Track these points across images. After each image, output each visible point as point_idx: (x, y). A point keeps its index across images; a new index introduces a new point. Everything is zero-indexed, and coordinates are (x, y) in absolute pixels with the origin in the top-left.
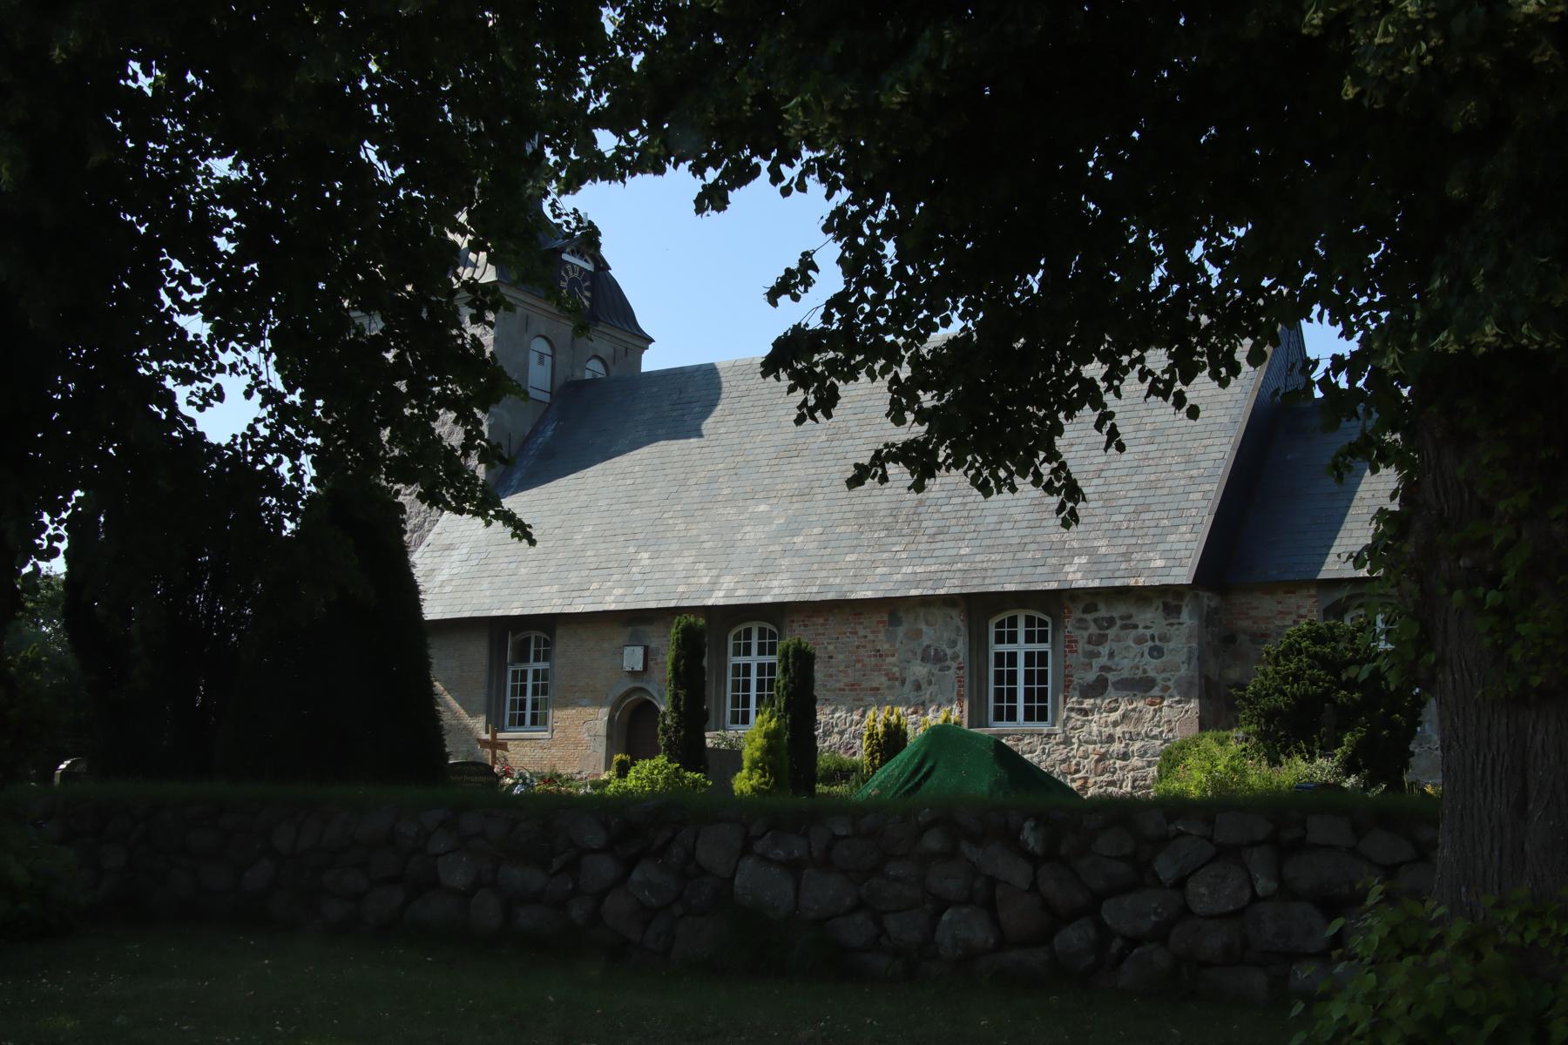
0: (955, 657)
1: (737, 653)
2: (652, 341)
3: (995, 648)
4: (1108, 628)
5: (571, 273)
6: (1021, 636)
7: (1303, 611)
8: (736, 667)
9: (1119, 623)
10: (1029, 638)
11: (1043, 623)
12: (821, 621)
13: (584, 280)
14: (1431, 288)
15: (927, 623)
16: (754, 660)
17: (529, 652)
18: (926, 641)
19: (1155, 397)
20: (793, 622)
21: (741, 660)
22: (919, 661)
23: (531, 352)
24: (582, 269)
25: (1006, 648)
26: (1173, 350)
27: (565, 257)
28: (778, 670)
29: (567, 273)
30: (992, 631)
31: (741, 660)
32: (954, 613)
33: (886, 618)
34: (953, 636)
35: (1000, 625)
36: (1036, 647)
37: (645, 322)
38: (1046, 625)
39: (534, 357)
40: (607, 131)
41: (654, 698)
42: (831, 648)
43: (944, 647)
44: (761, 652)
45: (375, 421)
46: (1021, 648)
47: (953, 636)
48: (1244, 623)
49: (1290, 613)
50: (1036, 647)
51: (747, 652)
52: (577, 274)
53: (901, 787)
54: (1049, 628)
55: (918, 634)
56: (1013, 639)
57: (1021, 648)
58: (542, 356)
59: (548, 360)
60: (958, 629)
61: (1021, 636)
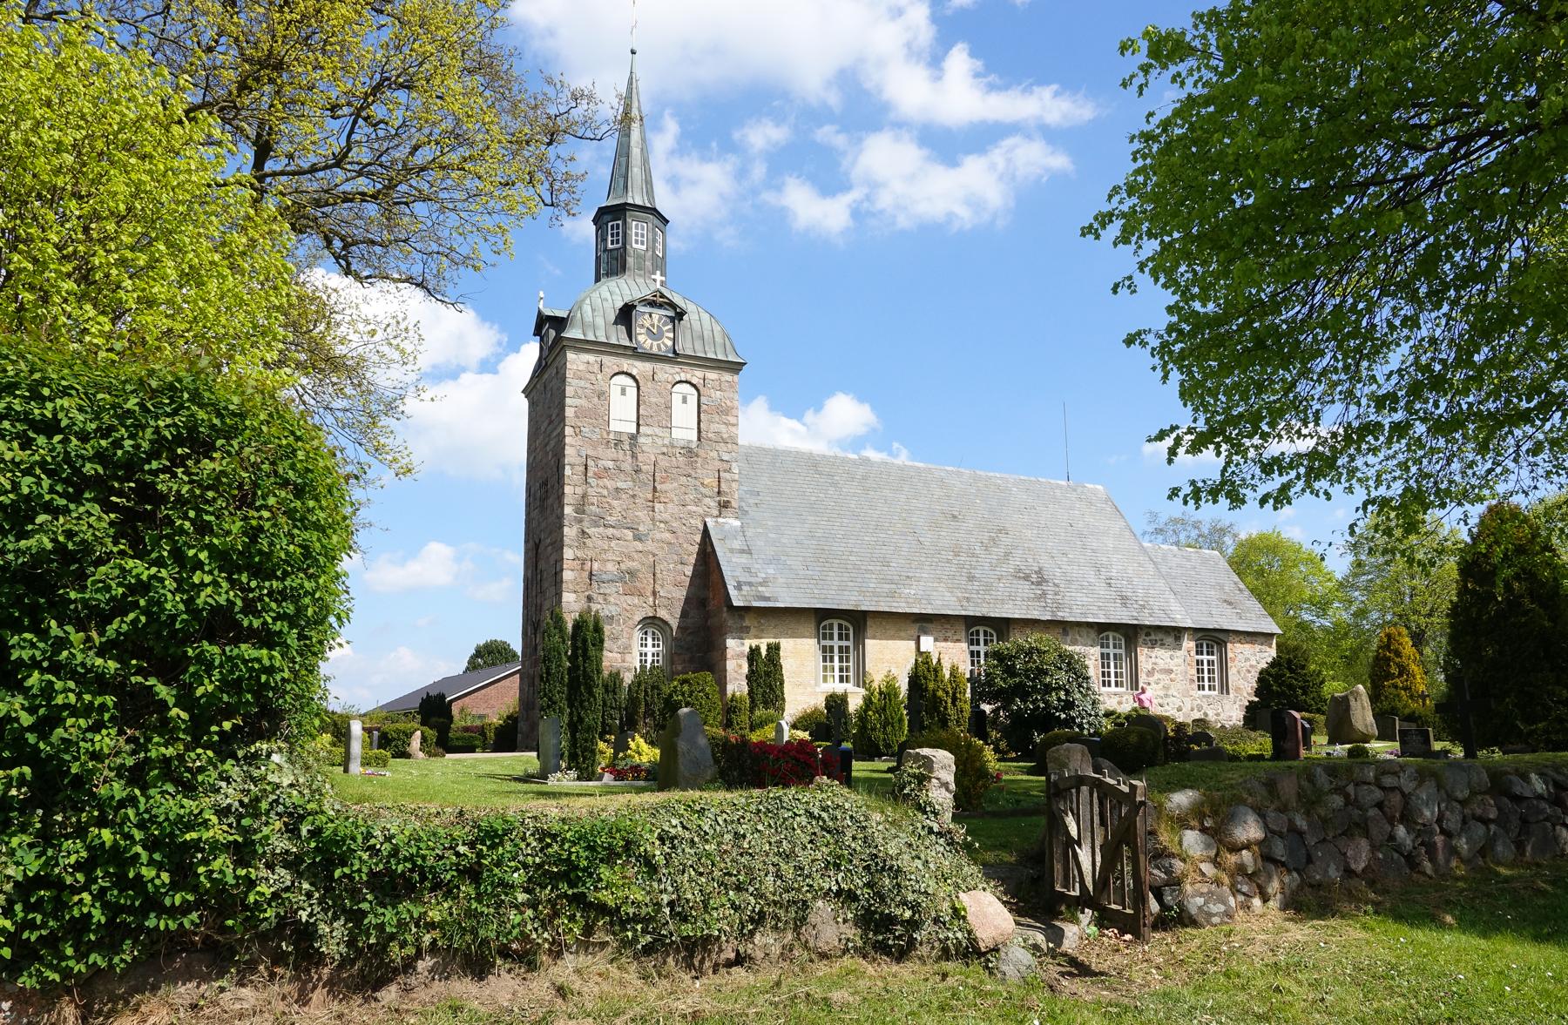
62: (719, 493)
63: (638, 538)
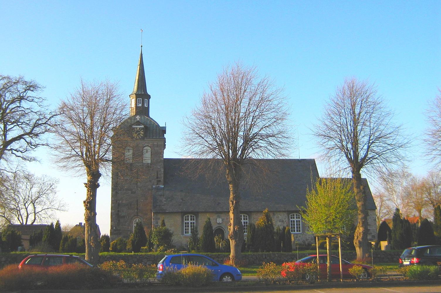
0: (286, 221)
3: (185, 221)
6: (190, 219)
10: (297, 218)
11: (299, 215)
15: (280, 215)
17: (302, 228)
18: (280, 218)
19: (49, 224)
20: (253, 214)
22: (279, 222)
25: (187, 221)
26: (207, 264)
28: (134, 223)
32: (285, 213)
33: (272, 214)
34: (285, 217)
35: (186, 217)
36: (298, 219)
38: (299, 216)
41: (223, 228)
43: (283, 219)
46: (295, 219)
47: (285, 217)
50: (298, 219)
53: (216, 228)
54: (195, 218)
56: (294, 218)
57: (295, 219)
60: (286, 217)
61: (190, 219)
62: (157, 178)
63: (132, 193)
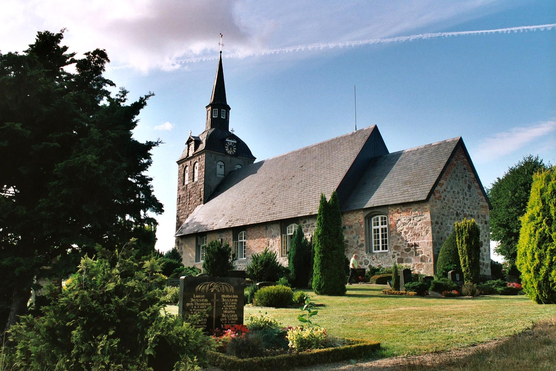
1: (375, 225)
2: (256, 158)
3: (374, 227)
4: (308, 227)
5: (229, 144)
6: (380, 224)
7: (360, 218)
8: (375, 230)
9: (311, 226)
12: (253, 230)
13: (234, 145)
14: (266, 51)
16: (380, 227)
21: (376, 227)
23: (217, 166)
24: (233, 143)
27: (227, 140)
29: (228, 144)
30: (373, 222)
31: (376, 227)
37: (254, 154)
39: (218, 167)
40: (228, 104)
42: (255, 237)
44: (382, 224)
45: (142, 186)
48: (347, 223)
49: (357, 219)
51: (378, 225)
52: (231, 144)
55: (271, 232)
58: (221, 166)
59: (223, 167)
61: (380, 224)
